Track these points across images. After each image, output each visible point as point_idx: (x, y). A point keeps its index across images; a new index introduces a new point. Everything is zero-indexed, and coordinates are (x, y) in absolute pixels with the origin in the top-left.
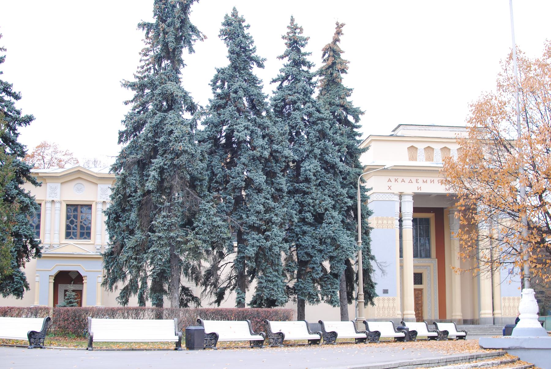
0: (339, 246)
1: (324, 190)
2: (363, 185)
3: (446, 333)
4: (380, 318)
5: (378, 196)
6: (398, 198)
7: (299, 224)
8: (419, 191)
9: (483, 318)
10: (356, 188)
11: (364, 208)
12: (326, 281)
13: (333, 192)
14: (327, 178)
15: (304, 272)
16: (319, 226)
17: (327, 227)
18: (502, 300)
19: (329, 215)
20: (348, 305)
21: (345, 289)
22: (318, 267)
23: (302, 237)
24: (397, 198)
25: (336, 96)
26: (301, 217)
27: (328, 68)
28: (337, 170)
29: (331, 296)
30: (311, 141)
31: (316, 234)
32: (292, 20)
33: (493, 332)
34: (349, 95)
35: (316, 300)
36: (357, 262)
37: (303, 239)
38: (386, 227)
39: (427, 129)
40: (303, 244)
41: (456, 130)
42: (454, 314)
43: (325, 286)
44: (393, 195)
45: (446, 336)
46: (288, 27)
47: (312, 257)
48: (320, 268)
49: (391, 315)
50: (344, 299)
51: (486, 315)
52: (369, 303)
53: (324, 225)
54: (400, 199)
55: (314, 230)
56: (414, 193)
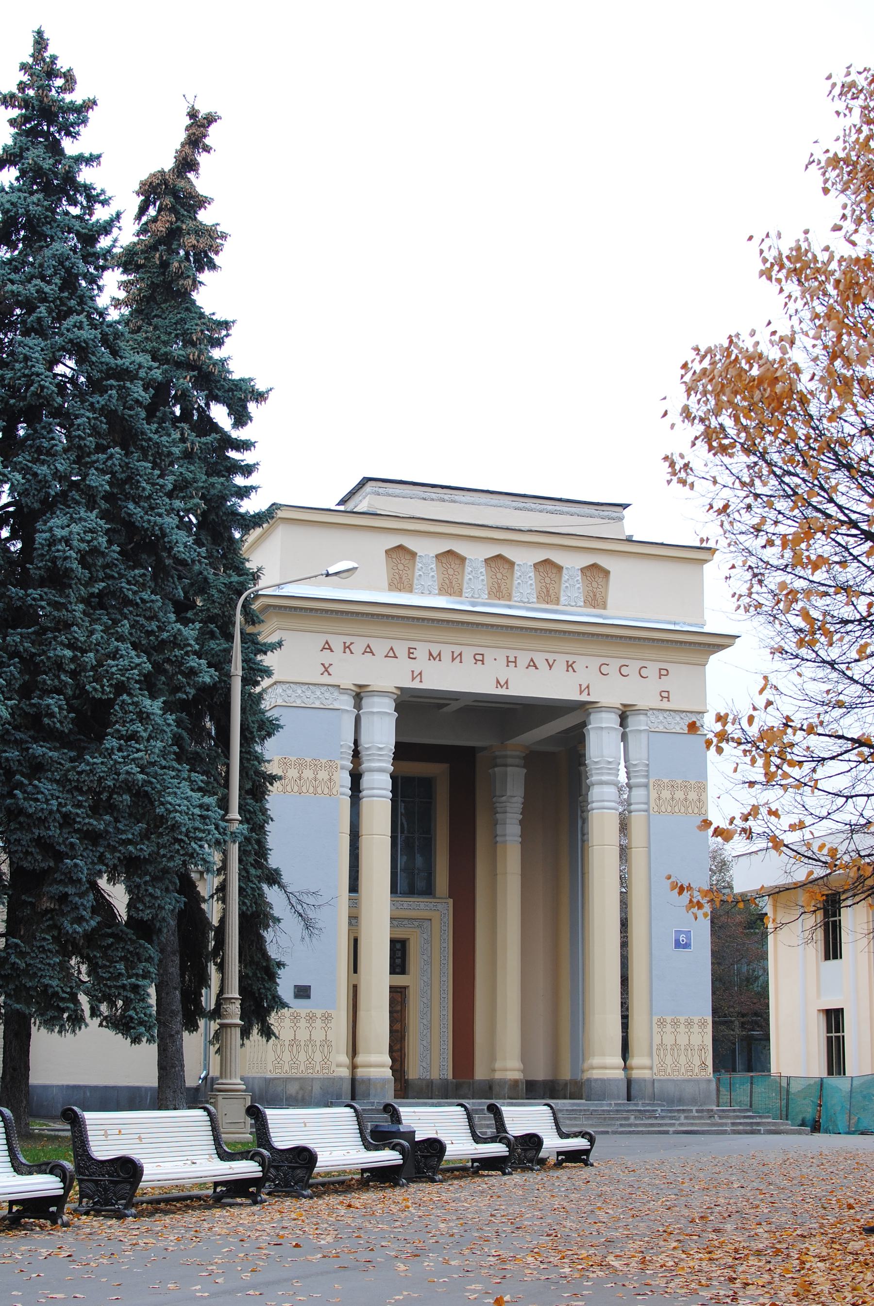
0: (162, 819)
1: (115, 622)
2: (250, 629)
3: (533, 1141)
4: (283, 1075)
5: (289, 692)
6: (352, 702)
7: (19, 735)
8: (416, 685)
9: (596, 1080)
10: (230, 638)
11: (251, 703)
12: (109, 946)
13: (149, 633)
14: (129, 583)
15: (28, 911)
16: (93, 746)
17: (120, 750)
18: (655, 1026)
19: (131, 708)
20: (186, 1034)
21: (177, 979)
22: (81, 895)
23: (26, 782)
24: (346, 703)
25: (177, 336)
26: (28, 709)
27: (154, 247)
28: (165, 554)
29: (127, 1002)
30: (80, 447)
31: (80, 773)
32: (40, 42)
33: (630, 1125)
34: (219, 343)
35: (69, 1018)
36: (222, 888)
37: (30, 789)
38: (311, 790)
39: (446, 497)
40: (31, 807)
41: (533, 506)
42: (498, 1065)
43: (104, 967)
44: (336, 694)
45: (530, 1154)
46: (24, 67)
47: (59, 857)
48: (90, 900)
49: (318, 1068)
50: (173, 1014)
51: (607, 1071)
52: (255, 1031)
53: (110, 742)
54: (358, 706)
55: (72, 760)
56: (401, 689)
